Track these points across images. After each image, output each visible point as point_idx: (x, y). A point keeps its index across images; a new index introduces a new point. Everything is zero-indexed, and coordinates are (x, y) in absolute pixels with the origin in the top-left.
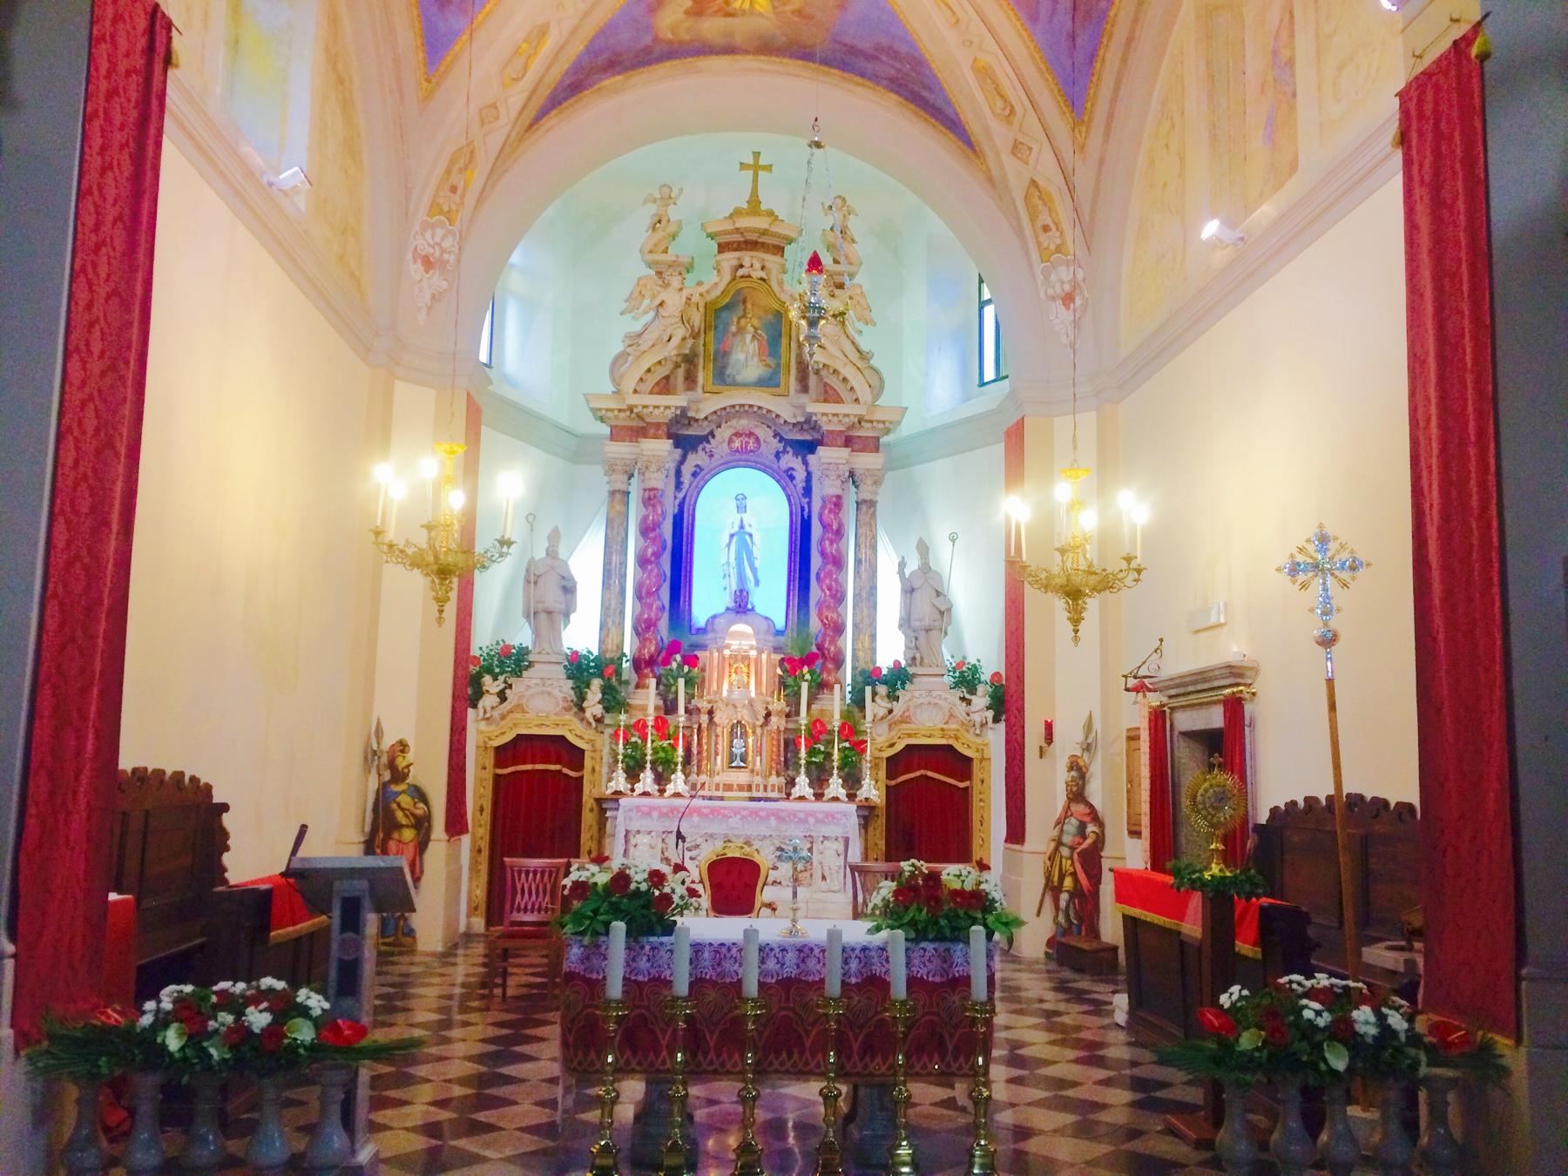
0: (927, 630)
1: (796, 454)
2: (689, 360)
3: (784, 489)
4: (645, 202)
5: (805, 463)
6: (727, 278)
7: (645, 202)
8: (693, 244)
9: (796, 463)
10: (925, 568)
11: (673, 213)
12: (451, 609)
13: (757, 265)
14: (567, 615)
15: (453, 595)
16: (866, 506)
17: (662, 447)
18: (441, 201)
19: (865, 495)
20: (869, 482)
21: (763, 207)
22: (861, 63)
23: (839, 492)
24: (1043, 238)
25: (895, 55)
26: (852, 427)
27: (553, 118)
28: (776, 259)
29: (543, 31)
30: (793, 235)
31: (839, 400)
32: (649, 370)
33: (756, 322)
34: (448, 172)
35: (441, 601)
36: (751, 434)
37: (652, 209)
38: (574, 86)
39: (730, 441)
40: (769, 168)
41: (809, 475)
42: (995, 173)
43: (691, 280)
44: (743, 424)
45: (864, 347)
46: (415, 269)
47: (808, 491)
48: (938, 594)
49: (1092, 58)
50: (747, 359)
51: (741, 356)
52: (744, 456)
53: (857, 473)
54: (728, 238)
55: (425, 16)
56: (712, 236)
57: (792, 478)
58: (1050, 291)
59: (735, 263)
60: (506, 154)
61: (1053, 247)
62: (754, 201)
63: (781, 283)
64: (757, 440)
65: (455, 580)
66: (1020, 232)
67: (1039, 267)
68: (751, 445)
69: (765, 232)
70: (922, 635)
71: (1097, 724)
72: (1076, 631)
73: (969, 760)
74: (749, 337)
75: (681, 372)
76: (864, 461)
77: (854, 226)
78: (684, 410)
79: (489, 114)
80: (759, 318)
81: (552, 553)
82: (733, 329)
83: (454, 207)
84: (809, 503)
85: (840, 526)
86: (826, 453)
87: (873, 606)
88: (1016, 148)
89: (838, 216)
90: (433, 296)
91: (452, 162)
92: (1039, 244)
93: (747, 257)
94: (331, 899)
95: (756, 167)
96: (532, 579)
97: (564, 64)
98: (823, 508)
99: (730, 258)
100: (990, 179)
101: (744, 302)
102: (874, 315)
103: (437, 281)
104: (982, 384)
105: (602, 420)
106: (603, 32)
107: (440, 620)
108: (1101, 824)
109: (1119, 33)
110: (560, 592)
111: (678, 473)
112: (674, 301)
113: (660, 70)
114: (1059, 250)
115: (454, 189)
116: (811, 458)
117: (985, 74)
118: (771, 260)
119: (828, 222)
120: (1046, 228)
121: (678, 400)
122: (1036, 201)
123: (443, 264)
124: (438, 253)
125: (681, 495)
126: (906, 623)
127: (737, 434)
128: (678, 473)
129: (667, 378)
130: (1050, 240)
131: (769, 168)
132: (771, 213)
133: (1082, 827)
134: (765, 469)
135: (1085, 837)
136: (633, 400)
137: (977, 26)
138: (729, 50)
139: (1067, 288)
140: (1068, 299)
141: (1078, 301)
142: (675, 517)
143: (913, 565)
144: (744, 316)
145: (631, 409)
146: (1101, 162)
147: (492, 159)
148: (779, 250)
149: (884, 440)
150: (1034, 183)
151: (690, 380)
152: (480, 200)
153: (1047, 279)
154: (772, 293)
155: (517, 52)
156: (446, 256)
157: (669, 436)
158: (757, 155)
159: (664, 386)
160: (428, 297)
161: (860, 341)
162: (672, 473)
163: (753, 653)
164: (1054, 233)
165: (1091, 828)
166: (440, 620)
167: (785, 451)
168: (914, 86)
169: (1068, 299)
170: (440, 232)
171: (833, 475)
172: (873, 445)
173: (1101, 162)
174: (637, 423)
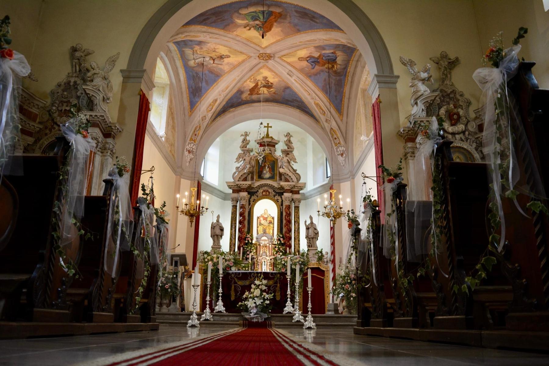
0: (313, 238)
2: (252, 173)
5: (281, 198)
8: (253, 145)
9: (279, 198)
10: (312, 223)
11: (248, 138)
12: (194, 224)
14: (221, 236)
15: (194, 221)
16: (297, 208)
17: (244, 194)
19: (296, 205)
22: (290, 103)
24: (335, 141)
25: (297, 101)
26: (292, 188)
27: (218, 118)
29: (216, 100)
31: (289, 181)
34: (194, 131)
35: (191, 222)
36: (267, 191)
37: (243, 137)
38: (215, 119)
40: (271, 127)
41: (282, 201)
43: (252, 154)
45: (295, 168)
46: (186, 153)
47: (282, 205)
48: (315, 229)
49: (341, 101)
51: (265, 172)
55: (190, 99)
60: (208, 126)
62: (268, 135)
64: (269, 192)
65: (195, 218)
68: (268, 194)
69: (270, 142)
70: (311, 240)
73: (324, 271)
75: (250, 176)
76: (296, 196)
77: (292, 139)
78: (250, 185)
79: (204, 118)
81: (218, 221)
85: (290, 212)
86: (289, 196)
87: (299, 233)
88: (326, 121)
91: (195, 129)
95: (268, 127)
96: (213, 227)
97: (221, 107)
100: (322, 128)
103: (191, 156)
104: (327, 177)
105: (230, 188)
106: (230, 100)
107: (191, 226)
109: (347, 95)
110: (219, 230)
111: (249, 201)
112: (247, 159)
113: (243, 106)
114: (339, 143)
116: (283, 196)
117: (317, 105)
118: (272, 148)
119: (286, 139)
120: (336, 139)
121: (249, 183)
123: (193, 152)
126: (307, 237)
127: (264, 191)
128: (249, 201)
129: (246, 177)
130: (337, 141)
131: (271, 127)
132: (272, 137)
134: (271, 199)
136: (238, 183)
137: (314, 95)
138: (259, 101)
140: (342, 155)
141: (344, 155)
143: (309, 222)
145: (237, 185)
146: (347, 123)
147: (204, 127)
148: (274, 146)
149: (300, 192)
151: (252, 179)
153: (337, 151)
155: (210, 105)
157: (247, 191)
158: (268, 124)
159: (245, 179)
161: (293, 166)
162: (248, 201)
163: (268, 245)
164: (337, 139)
166: (191, 226)
168: (302, 107)
169: (342, 155)
170: (192, 145)
172: (297, 192)
173: (347, 123)
174: (239, 189)
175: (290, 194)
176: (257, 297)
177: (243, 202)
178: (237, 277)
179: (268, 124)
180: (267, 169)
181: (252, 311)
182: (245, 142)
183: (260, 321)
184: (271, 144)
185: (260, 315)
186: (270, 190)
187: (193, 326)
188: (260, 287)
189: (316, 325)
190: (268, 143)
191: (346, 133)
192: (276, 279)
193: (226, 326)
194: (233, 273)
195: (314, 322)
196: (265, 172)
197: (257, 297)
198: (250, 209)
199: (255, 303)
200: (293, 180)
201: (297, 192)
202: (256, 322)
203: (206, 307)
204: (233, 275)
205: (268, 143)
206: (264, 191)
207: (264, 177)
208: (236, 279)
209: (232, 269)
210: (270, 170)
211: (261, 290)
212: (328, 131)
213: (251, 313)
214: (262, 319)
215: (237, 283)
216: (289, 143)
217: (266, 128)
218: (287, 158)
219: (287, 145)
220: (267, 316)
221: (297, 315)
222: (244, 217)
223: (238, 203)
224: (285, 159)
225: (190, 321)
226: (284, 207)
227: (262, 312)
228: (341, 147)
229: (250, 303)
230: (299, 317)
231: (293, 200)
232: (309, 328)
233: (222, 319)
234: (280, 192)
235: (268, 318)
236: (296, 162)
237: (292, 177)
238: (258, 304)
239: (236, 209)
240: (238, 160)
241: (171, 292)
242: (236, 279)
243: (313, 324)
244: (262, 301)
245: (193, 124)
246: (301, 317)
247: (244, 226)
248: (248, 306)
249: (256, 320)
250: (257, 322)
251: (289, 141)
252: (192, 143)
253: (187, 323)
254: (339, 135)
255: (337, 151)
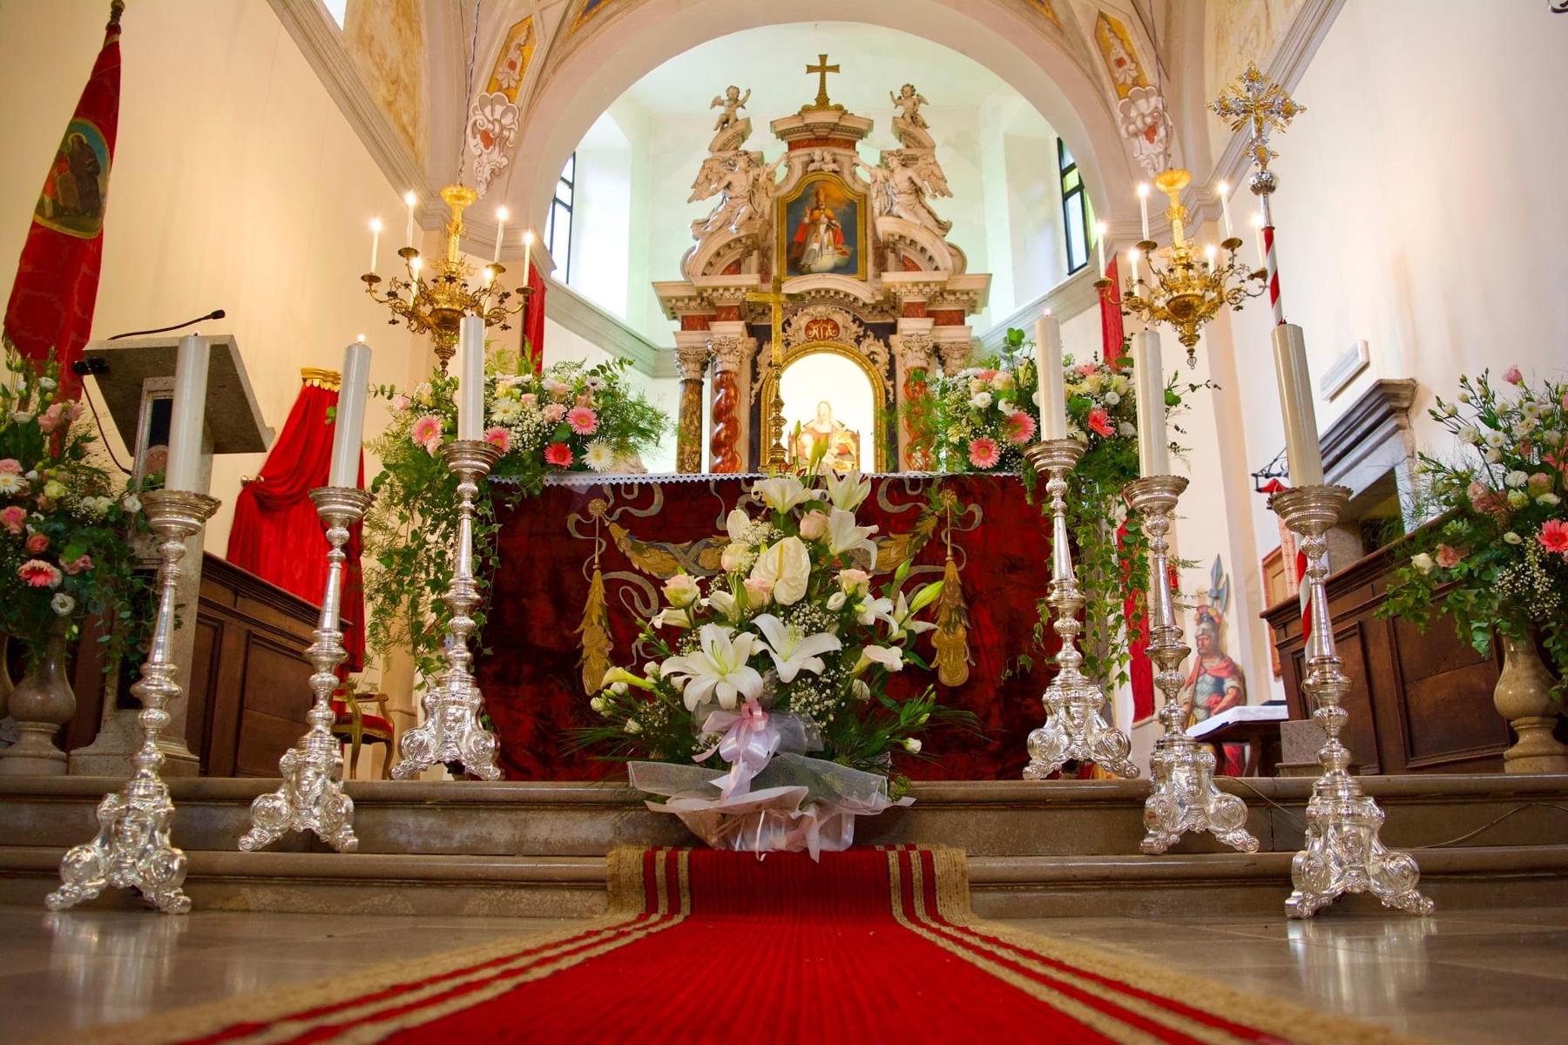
1: (877, 338)
3: (867, 372)
4: (714, 105)
5: (888, 345)
6: (798, 172)
7: (714, 105)
9: (879, 347)
11: (740, 114)
13: (828, 158)
18: (500, 77)
20: (956, 355)
21: (832, 103)
23: (924, 364)
24: (1120, 74)
26: (932, 299)
28: (848, 152)
30: (864, 127)
31: (918, 269)
32: (718, 254)
33: (829, 213)
36: (829, 320)
37: (720, 110)
39: (808, 328)
40: (836, 69)
42: (1062, 17)
44: (820, 310)
46: (474, 144)
47: (891, 374)
50: (823, 250)
51: (816, 246)
52: (824, 337)
53: (944, 346)
54: (794, 137)
56: (782, 135)
57: (874, 362)
58: (1132, 128)
59: (806, 159)
61: (1129, 81)
62: (822, 100)
63: (854, 175)
64: (836, 327)
66: (1093, 77)
67: (1117, 106)
68: (830, 332)
69: (834, 127)
71: (1227, 568)
72: (1191, 352)
74: (823, 228)
77: (922, 111)
80: (833, 209)
82: (807, 220)
83: (513, 84)
84: (894, 386)
89: (909, 103)
90: (493, 172)
92: (1114, 80)
93: (817, 153)
94: (138, 397)
95: (823, 68)
98: (908, 381)
99: (801, 154)
100: (1058, 27)
101: (817, 194)
102: (950, 186)
103: (496, 156)
108: (1242, 679)
111: (754, 364)
114: (1136, 82)
115: (512, 65)
116: (893, 339)
118: (841, 152)
119: (900, 111)
120: (1120, 62)
122: (1108, 35)
124: (497, 130)
125: (757, 386)
130: (1126, 74)
131: (836, 69)
132: (839, 108)
133: (1219, 682)
134: (846, 352)
135: (1222, 695)
139: (1149, 120)
140: (1150, 132)
141: (1162, 132)
142: (752, 408)
144: (818, 208)
147: (551, 32)
148: (851, 145)
150: (1102, 16)
152: (540, 83)
153: (1128, 119)
154: (843, 184)
156: (506, 133)
158: (823, 58)
159: (736, 268)
160: (487, 174)
164: (1129, 65)
165: (1229, 683)
167: (865, 336)
169: (1150, 132)
170: (499, 109)
171: (916, 347)
175: (928, 323)
176: (773, 608)
177: (726, 362)
178: (625, 520)
179: (823, 58)
180: (824, 234)
181: (728, 746)
182: (732, 129)
183: (816, 844)
184: (837, 135)
185: (815, 779)
186: (839, 318)
187: (124, 905)
188: (808, 525)
189: (1427, 877)
190: (823, 132)
191: (1167, 40)
192: (928, 525)
193: (478, 899)
194: (596, 491)
195: (1391, 837)
196: (816, 246)
197: (773, 608)
198: (758, 396)
199: (762, 662)
200: (938, 261)
201: (957, 318)
202: (775, 857)
203: (307, 727)
204: (596, 507)
205: (823, 132)
206: (815, 321)
207: (813, 267)
208: (619, 533)
209: (590, 459)
210: (836, 241)
211: (817, 550)
212: (1085, 26)
213: (719, 764)
214: (832, 829)
215: (626, 565)
216: (911, 127)
217: (817, 63)
218: (910, 172)
219: (903, 135)
220: (879, 802)
221: (1181, 776)
222: (732, 424)
223: (708, 373)
224: (901, 177)
225: (91, 853)
226: (901, 378)
227: (829, 754)
228: (1147, 95)
229: (712, 670)
230: (1197, 797)
231: (937, 348)
232: (1349, 910)
233: (464, 832)
234: (879, 325)
235: (894, 813)
236: (945, 193)
237: (931, 251)
238: (786, 671)
239: (700, 394)
240: (701, 188)
241: (74, 617)
242: (619, 533)
243: (1388, 870)
244: (830, 642)
245: (498, 12)
246: (1216, 801)
247: (733, 460)
248: (691, 698)
249: (780, 841)
250: (791, 862)
251: (914, 118)
252: (501, 102)
253: (51, 875)
254: (1136, 39)
255: (1128, 119)
